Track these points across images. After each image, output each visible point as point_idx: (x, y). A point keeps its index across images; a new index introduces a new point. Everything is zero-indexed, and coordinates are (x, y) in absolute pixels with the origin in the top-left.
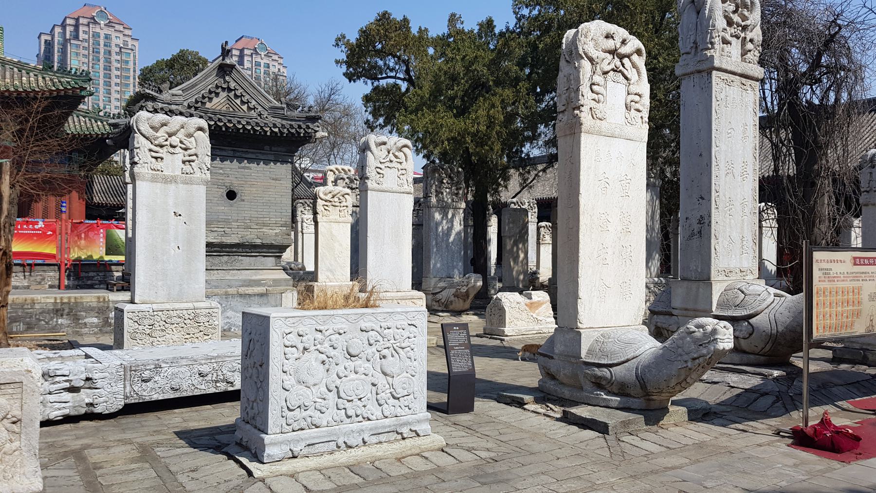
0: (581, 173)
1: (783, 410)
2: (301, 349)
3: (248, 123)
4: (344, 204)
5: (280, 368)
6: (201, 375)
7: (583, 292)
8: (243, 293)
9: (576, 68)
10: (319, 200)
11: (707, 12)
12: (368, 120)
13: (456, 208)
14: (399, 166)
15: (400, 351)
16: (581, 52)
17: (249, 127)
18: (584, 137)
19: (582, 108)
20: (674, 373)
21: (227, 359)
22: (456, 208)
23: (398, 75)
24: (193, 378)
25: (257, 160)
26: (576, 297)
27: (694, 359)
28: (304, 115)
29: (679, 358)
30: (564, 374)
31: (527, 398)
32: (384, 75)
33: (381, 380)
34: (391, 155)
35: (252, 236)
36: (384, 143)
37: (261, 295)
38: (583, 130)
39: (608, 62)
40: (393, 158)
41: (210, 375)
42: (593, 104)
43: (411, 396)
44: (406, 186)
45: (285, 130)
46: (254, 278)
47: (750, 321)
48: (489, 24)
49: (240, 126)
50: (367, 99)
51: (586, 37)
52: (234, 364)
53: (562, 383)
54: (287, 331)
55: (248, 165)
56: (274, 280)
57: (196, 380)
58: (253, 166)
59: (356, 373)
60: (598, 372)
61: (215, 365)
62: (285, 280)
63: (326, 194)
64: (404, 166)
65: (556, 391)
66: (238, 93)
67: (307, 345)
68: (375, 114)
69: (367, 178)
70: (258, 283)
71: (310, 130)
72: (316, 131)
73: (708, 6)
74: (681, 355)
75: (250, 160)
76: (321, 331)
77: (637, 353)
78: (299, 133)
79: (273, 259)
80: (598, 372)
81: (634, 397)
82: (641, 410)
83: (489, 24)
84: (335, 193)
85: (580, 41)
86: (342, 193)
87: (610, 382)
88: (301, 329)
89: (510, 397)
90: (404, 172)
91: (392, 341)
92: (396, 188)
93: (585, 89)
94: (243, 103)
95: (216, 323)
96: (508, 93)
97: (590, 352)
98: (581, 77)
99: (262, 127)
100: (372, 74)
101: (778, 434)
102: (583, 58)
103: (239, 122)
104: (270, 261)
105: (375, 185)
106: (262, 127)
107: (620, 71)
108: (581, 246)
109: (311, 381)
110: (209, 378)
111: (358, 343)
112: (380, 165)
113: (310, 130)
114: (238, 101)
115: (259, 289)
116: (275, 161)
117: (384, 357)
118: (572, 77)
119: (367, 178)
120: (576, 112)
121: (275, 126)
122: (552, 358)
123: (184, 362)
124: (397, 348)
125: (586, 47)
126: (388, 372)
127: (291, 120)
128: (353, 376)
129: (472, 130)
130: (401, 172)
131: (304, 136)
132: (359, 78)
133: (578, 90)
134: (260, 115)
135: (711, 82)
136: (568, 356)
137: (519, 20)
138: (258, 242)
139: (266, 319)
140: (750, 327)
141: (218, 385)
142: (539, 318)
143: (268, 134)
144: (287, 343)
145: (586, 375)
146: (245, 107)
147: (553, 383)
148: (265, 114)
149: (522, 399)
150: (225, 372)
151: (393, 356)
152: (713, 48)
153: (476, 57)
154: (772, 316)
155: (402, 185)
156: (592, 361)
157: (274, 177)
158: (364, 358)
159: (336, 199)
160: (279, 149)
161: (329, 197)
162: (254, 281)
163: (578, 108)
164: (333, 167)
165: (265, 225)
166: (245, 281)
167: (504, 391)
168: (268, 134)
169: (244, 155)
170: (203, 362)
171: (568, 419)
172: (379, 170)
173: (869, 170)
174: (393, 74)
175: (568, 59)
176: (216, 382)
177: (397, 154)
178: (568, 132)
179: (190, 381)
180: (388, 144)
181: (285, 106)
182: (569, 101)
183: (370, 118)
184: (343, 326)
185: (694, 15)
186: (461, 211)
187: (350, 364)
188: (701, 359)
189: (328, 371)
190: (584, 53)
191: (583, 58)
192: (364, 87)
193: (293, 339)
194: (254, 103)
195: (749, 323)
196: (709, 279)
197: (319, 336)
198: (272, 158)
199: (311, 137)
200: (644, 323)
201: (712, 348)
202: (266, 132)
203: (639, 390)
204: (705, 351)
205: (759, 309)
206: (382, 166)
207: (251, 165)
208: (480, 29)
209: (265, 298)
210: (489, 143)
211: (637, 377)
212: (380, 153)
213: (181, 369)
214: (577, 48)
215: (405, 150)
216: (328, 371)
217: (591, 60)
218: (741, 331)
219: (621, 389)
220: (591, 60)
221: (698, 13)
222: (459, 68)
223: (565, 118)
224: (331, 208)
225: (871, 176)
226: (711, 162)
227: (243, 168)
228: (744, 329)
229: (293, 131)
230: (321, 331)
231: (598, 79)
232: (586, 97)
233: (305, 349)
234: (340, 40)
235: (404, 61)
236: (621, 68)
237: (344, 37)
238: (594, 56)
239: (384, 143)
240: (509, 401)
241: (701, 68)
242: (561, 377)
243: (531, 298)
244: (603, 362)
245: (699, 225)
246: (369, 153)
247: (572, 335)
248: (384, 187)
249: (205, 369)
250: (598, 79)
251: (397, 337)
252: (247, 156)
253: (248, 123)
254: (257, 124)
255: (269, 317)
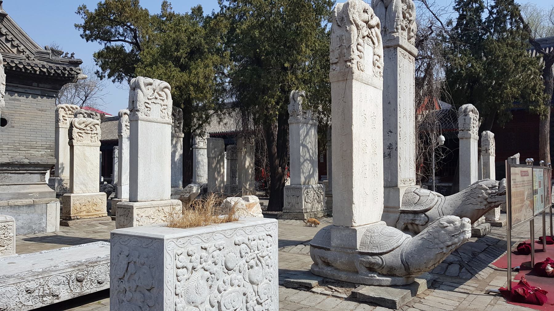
0: (354, 109)
1: (469, 274)
2: (190, 268)
3: (20, 63)
4: (95, 132)
5: (173, 291)
6: (28, 292)
7: (356, 199)
8: (13, 204)
9: (347, 31)
10: (74, 128)
11: (394, 7)
12: (98, 72)
13: (178, 137)
14: (161, 102)
15: (261, 258)
16: (351, 19)
17: (21, 66)
18: (354, 82)
19: (352, 61)
20: (432, 257)
21: (53, 273)
22: (178, 137)
23: (127, 39)
24: (20, 296)
25: (27, 94)
26: (351, 202)
27: (448, 246)
28: (68, 60)
29: (436, 246)
30: (341, 262)
31: (314, 282)
32: (116, 39)
33: (249, 289)
34: (156, 93)
35: (21, 157)
36: (151, 84)
37: (29, 206)
38: (354, 77)
39: (365, 31)
40: (157, 96)
41: (37, 291)
42: (358, 59)
43: (269, 300)
44: (167, 118)
45: (53, 71)
46: (22, 191)
47: (426, 213)
48: (198, 10)
49: (14, 65)
50: (99, 55)
51: (354, 9)
52: (59, 278)
53: (337, 269)
54: (179, 253)
55: (18, 98)
56: (40, 193)
57: (24, 296)
58: (23, 98)
59: (232, 285)
60: (372, 259)
61: (42, 280)
62: (50, 192)
63: (80, 124)
64: (165, 102)
65: (333, 275)
66: (9, 37)
67: (195, 264)
68: (104, 68)
69: (138, 111)
70: (25, 196)
71: (73, 72)
72: (78, 73)
73: (394, 4)
74: (437, 244)
75: (20, 94)
76: (205, 249)
77: (399, 243)
78: (64, 74)
79: (39, 175)
80: (372, 259)
81: (398, 276)
82: (403, 286)
83: (198, 10)
84: (88, 123)
85: (350, 11)
86: (94, 123)
87: (381, 266)
88: (191, 249)
89: (297, 283)
90: (165, 107)
91: (257, 252)
92: (160, 119)
93: (354, 46)
94: (13, 46)
95: (11, 234)
96: (216, 58)
97: (362, 244)
98: (352, 38)
99: (32, 67)
100: (106, 37)
101: (488, 294)
102: (352, 24)
103: (12, 62)
104: (36, 178)
105: (144, 117)
106: (32, 67)
107: (370, 38)
108: (354, 164)
109: (198, 299)
110: (36, 294)
111: (232, 256)
112: (148, 101)
113: (73, 72)
114: (9, 45)
115: (27, 200)
116: (42, 96)
117: (252, 267)
118: (344, 37)
119: (138, 111)
120: (349, 64)
121: (43, 66)
122: (329, 250)
123: (11, 281)
124: (259, 257)
125: (354, 16)
126: (255, 281)
127: (52, 63)
128: (230, 289)
129: (195, 82)
130: (163, 107)
131: (68, 77)
132: (96, 39)
133: (349, 47)
134: (28, 58)
135: (396, 55)
136: (345, 248)
137: (222, 9)
138: (26, 161)
139: (162, 241)
140: (426, 218)
141: (45, 299)
142: (254, 215)
143: (38, 73)
144: (180, 265)
145: (362, 262)
146: (15, 50)
147: (329, 269)
148: (32, 57)
149: (310, 284)
150: (51, 286)
151: (257, 265)
152: (397, 32)
153: (196, 30)
154: (440, 210)
155: (163, 117)
156: (366, 251)
157: (40, 108)
158: (237, 271)
159: (88, 128)
160: (46, 86)
161: (82, 126)
162: (22, 194)
163: (350, 61)
164: (64, 105)
165: (32, 147)
166: (14, 194)
167: (288, 278)
168: (38, 73)
169: (14, 90)
170: (30, 279)
171: (355, 298)
172: (147, 105)
173: (464, 117)
174: (123, 38)
175: (339, 24)
176: (43, 296)
177: (160, 93)
178: (340, 79)
179: (17, 300)
180: (154, 84)
181: (50, 52)
182: (341, 55)
183: (100, 70)
184: (221, 242)
185: (384, 9)
186: (182, 139)
187: (227, 278)
188: (453, 246)
189: (210, 287)
190: (354, 20)
191: (352, 24)
192: (98, 46)
193: (184, 260)
194: (22, 47)
195: (425, 215)
196: (397, 186)
197: (204, 253)
198: (39, 93)
199: (73, 78)
200: (382, 219)
201: (462, 238)
202: (36, 71)
203: (403, 271)
204: (456, 240)
205: (431, 205)
206: (149, 102)
207: (21, 98)
208: (192, 13)
209: (32, 208)
210: (205, 92)
211: (402, 261)
212: (148, 92)
213: (9, 288)
214: (348, 16)
215: (166, 90)
216: (210, 287)
217: (357, 26)
218: (420, 220)
219: (390, 272)
220: (357, 26)
221: (386, 8)
222: (184, 37)
223: (338, 68)
224: (84, 135)
225: (465, 121)
226: (397, 108)
227: (13, 100)
228: (422, 219)
229: (59, 72)
230: (205, 249)
231: (361, 41)
232: (355, 55)
233: (194, 268)
234: (82, 9)
235: (132, 30)
236: (371, 35)
237: (85, 7)
238: (359, 24)
239: (151, 84)
240: (297, 286)
241: (390, 45)
242: (338, 264)
243: (248, 201)
244: (375, 252)
245: (389, 150)
246: (139, 91)
247: (347, 232)
248: (151, 118)
249: (32, 285)
250: (361, 41)
251: (260, 247)
252: (17, 90)
253: (20, 63)
254: (29, 64)
255: (163, 240)
